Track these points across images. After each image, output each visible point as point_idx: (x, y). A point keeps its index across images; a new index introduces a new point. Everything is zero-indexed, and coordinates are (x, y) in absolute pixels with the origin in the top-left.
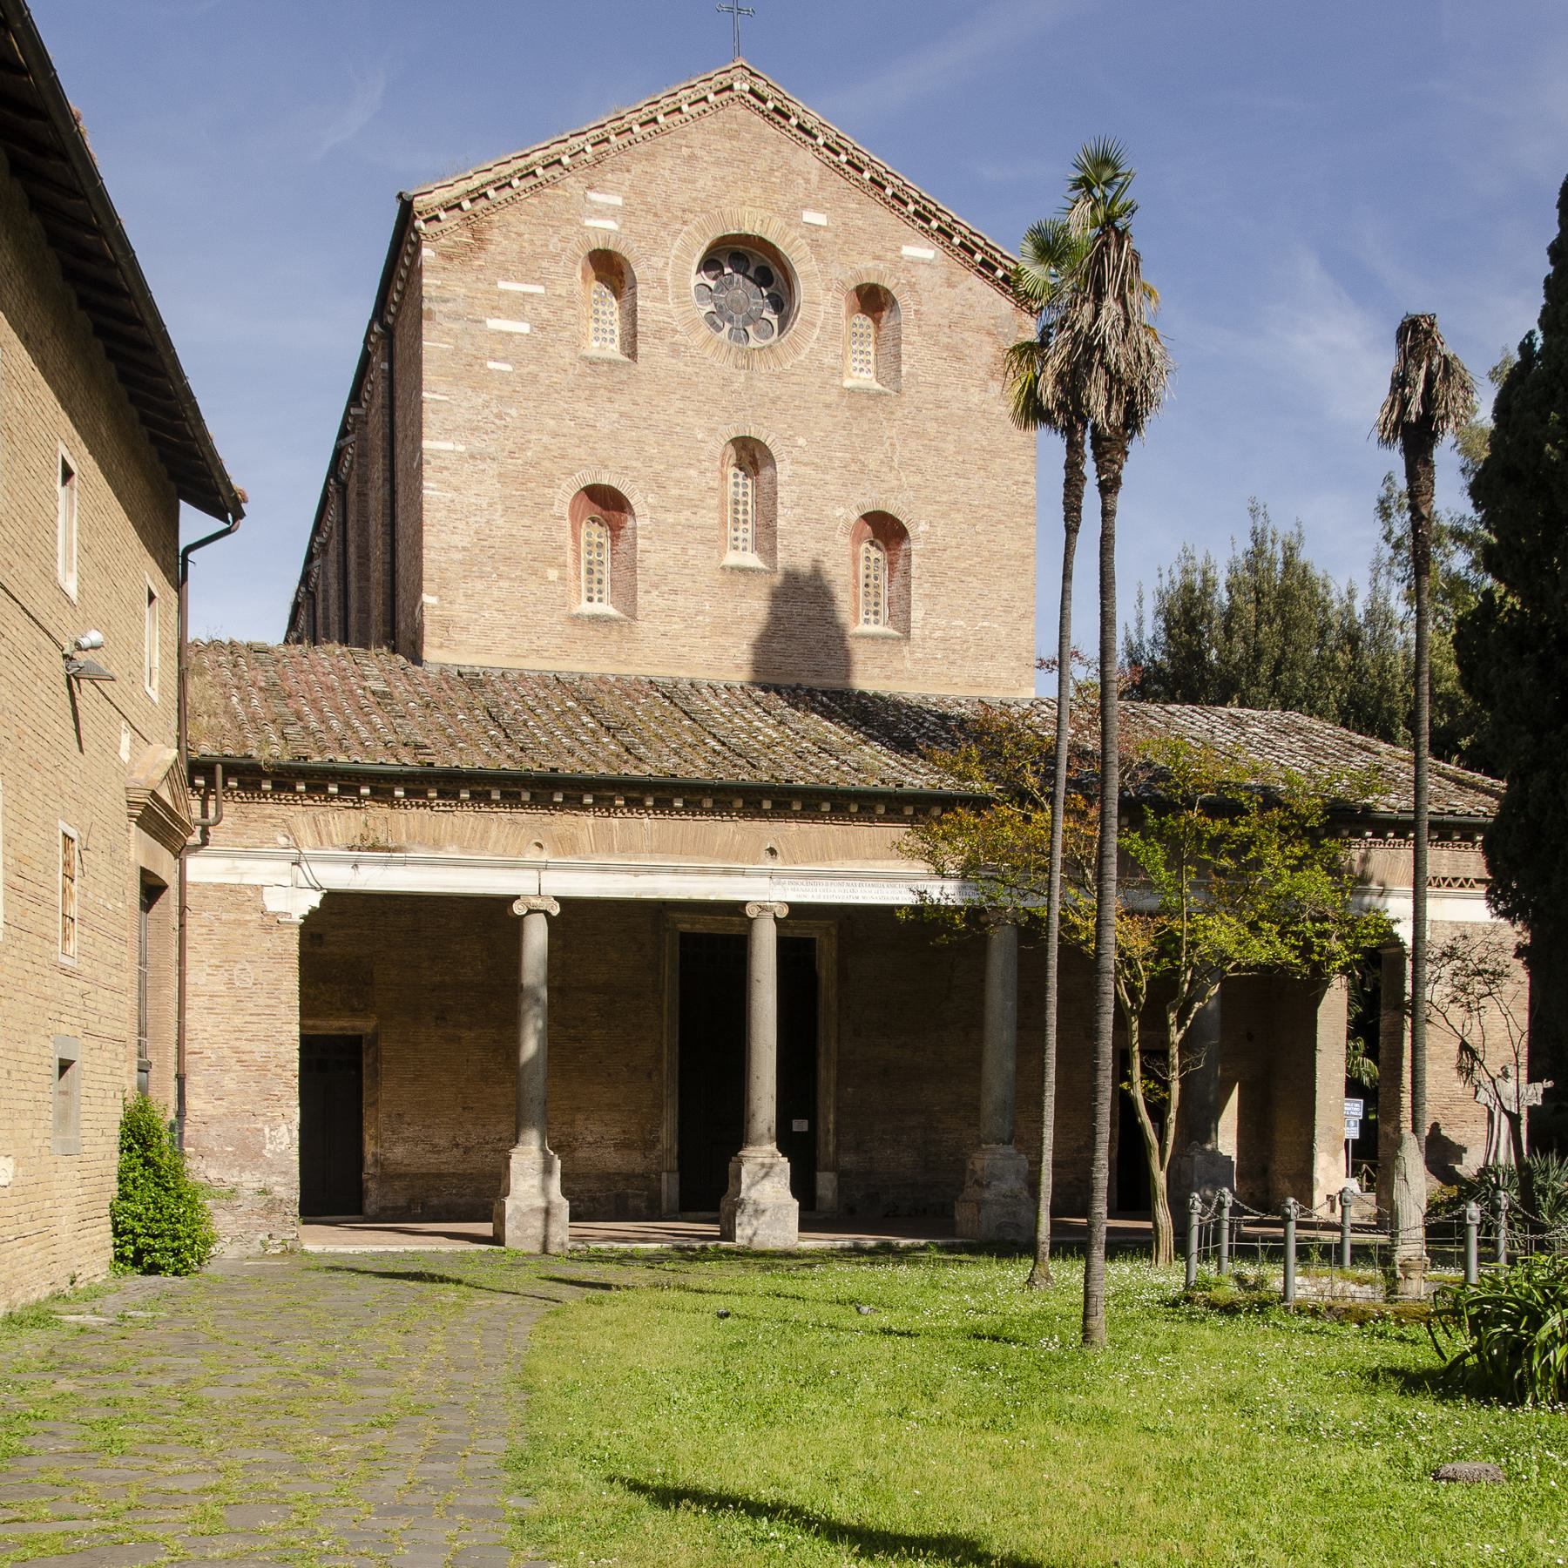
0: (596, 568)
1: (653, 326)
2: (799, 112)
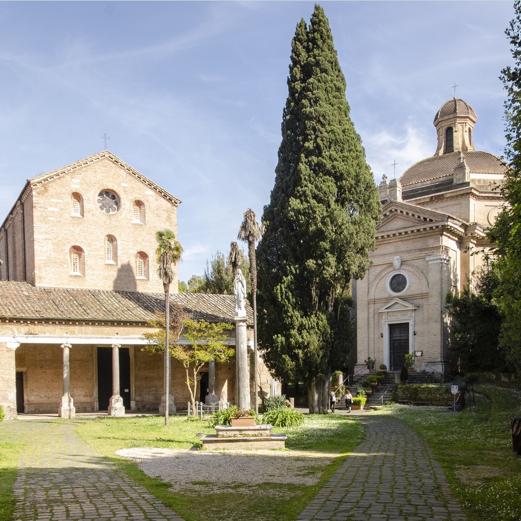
0: (75, 264)
1: (88, 210)
2: (120, 161)
